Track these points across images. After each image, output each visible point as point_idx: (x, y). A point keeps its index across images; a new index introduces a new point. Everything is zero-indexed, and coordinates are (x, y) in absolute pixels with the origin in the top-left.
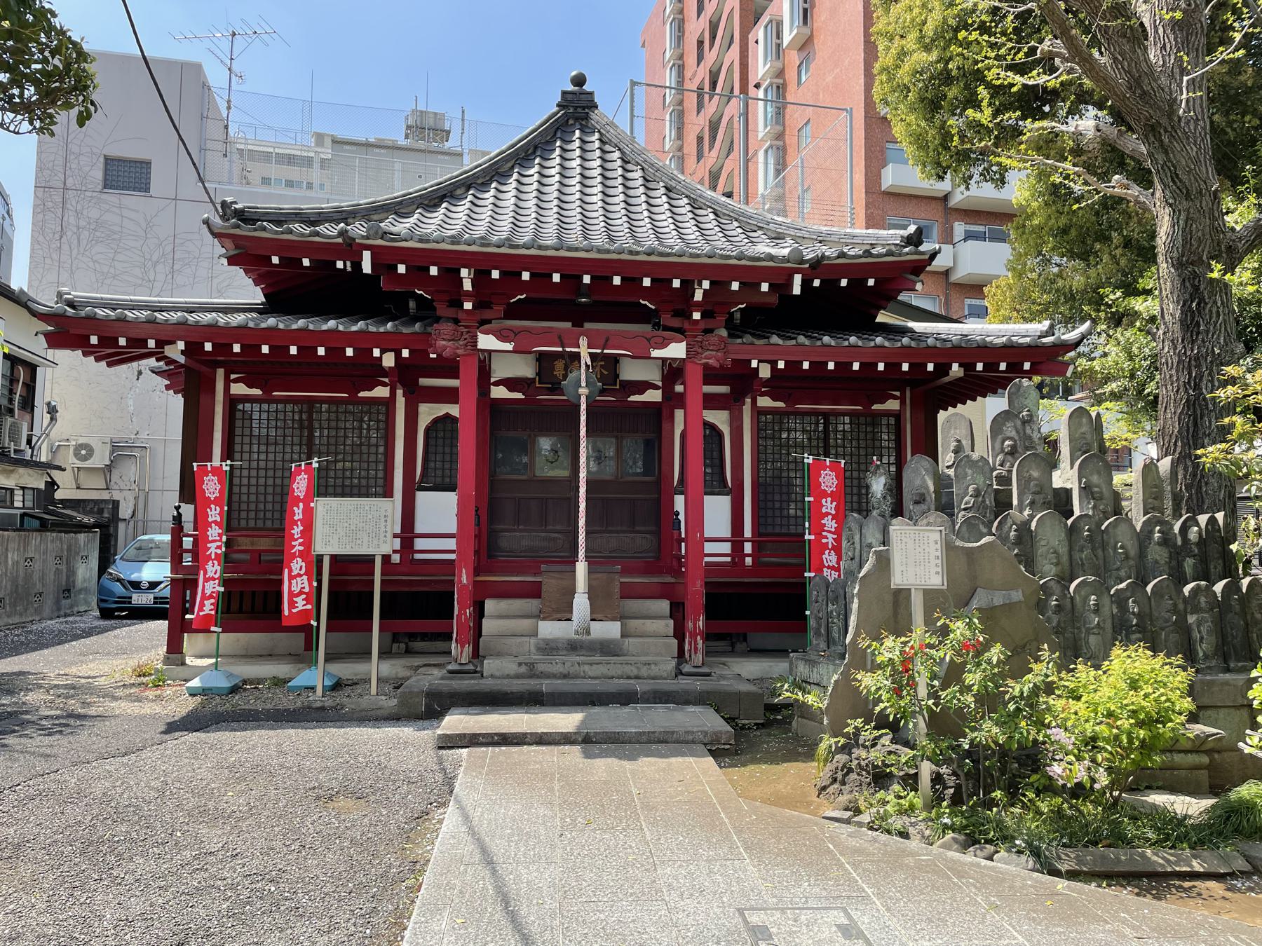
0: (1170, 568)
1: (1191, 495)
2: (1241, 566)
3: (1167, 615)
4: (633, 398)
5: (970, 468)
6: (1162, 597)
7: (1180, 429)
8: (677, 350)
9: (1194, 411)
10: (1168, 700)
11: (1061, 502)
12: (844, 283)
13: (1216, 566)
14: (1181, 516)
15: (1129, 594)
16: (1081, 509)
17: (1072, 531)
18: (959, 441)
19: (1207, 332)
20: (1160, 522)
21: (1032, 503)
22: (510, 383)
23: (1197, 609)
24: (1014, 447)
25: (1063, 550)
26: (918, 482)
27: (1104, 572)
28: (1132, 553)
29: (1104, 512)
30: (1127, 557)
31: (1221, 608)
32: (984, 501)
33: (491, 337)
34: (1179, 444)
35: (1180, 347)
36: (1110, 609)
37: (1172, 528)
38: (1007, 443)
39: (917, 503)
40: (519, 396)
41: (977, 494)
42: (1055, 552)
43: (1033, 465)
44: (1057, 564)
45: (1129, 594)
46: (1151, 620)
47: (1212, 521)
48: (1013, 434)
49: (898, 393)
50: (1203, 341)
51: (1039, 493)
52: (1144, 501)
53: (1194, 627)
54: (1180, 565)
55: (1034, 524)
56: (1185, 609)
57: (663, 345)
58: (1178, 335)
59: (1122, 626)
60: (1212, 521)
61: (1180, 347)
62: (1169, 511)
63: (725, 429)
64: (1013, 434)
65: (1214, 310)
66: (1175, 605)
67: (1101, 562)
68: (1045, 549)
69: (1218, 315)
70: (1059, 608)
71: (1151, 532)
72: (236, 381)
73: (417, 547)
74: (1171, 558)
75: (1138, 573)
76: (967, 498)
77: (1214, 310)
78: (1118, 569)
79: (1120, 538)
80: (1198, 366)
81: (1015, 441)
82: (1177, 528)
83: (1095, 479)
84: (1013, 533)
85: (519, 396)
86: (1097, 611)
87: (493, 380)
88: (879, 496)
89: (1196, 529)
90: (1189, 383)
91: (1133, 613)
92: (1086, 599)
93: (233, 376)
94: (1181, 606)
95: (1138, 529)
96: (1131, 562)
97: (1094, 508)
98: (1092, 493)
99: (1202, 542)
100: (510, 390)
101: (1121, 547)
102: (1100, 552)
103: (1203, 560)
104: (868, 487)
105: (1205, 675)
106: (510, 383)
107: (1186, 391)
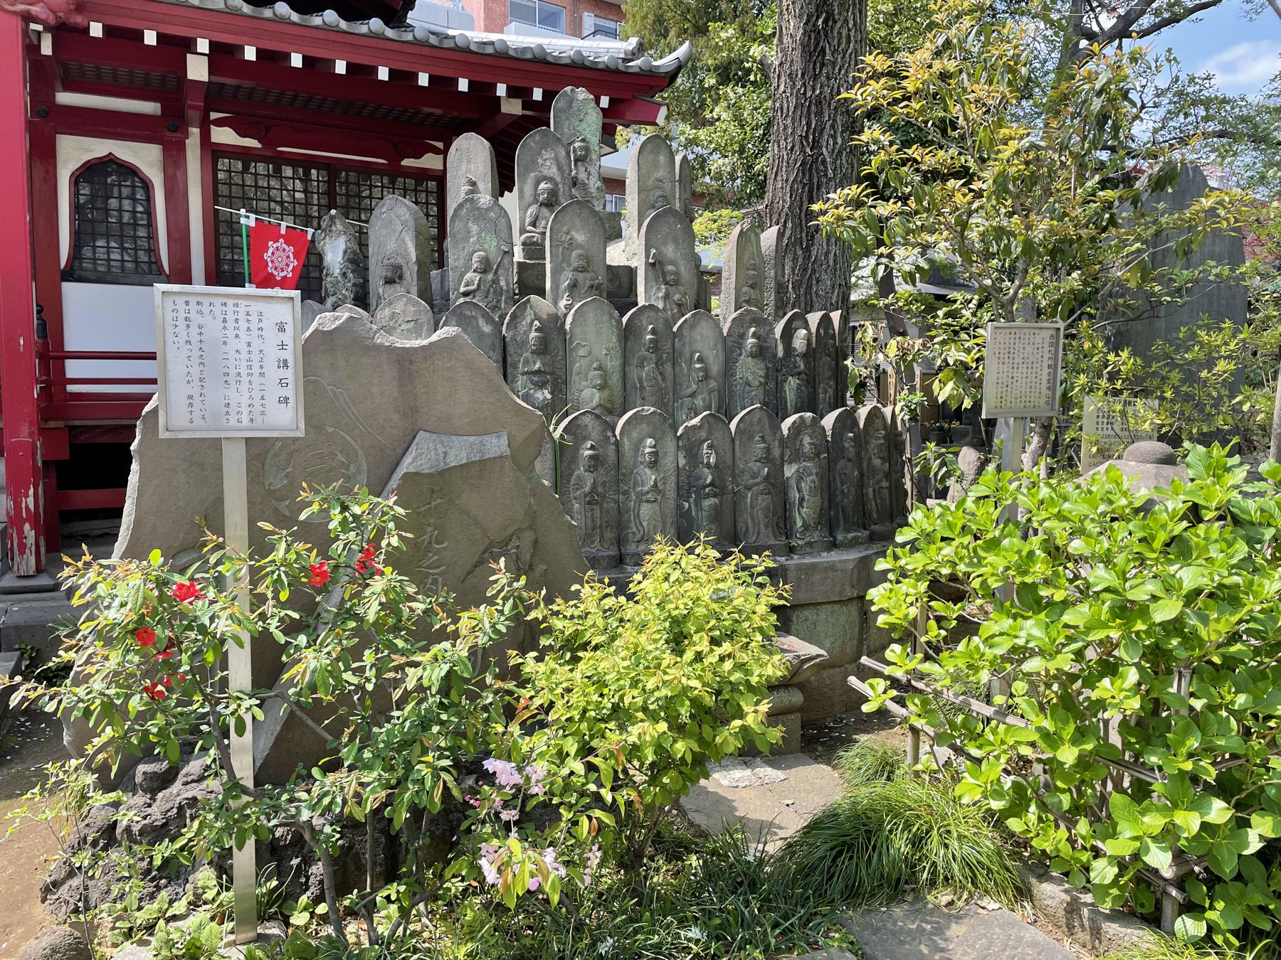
0: (766, 393)
1: (798, 296)
2: (852, 390)
3: (755, 466)
5: (476, 220)
6: (751, 437)
7: (792, 204)
9: (811, 179)
10: (740, 666)
11: (618, 289)
13: (825, 392)
14: (785, 314)
15: (703, 434)
16: (647, 298)
17: (628, 334)
18: (473, 184)
19: (834, 64)
20: (757, 321)
21: (573, 286)
23: (797, 456)
24: (553, 193)
25: (613, 364)
26: (391, 246)
27: (669, 404)
28: (715, 369)
29: (679, 305)
30: (707, 377)
31: (830, 451)
32: (495, 281)
34: (790, 225)
35: (799, 84)
36: (673, 458)
37: (772, 331)
38: (543, 186)
39: (389, 281)
41: (485, 267)
42: (600, 368)
43: (577, 222)
44: (601, 388)
45: (703, 434)
46: (733, 476)
47: (826, 321)
48: (553, 172)
49: (440, 145)
50: (828, 78)
51: (583, 270)
52: (738, 290)
53: (793, 483)
54: (779, 388)
55: (569, 319)
56: (782, 455)
58: (798, 66)
59: (690, 486)
60: (826, 321)
61: (799, 84)
62: (770, 309)
63: (98, 148)
64: (553, 172)
65: (844, 32)
66: (768, 450)
67: (669, 383)
68: (584, 362)
69: (849, 42)
70: (596, 462)
71: (743, 336)
73: (70, 374)
74: (767, 377)
75: (721, 400)
76: (469, 275)
77: (844, 32)
78: (693, 395)
79: (699, 345)
80: (819, 114)
81: (556, 184)
82: (779, 328)
83: (670, 251)
84: (533, 334)
86: (654, 464)
88: (337, 272)
89: (804, 332)
90: (806, 137)
91: (708, 465)
92: (638, 445)
94: (776, 452)
95: (725, 332)
96: (713, 384)
97: (667, 297)
98: (664, 274)
99: (810, 354)
101: (700, 360)
102: (668, 368)
103: (810, 381)
104: (320, 257)
105: (803, 555)
107: (803, 150)
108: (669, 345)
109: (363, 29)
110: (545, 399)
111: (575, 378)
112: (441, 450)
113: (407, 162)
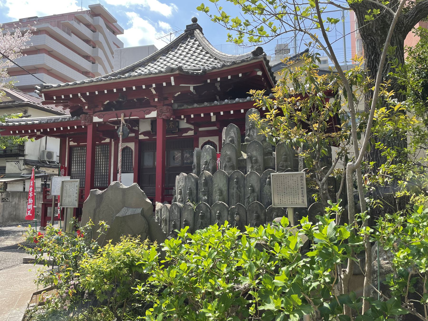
4: (184, 135)
6: (253, 212)
8: (154, 114)
12: (229, 77)
22: (145, 134)
25: (225, 189)
28: (257, 189)
33: (97, 117)
40: (147, 138)
51: (228, 162)
57: (149, 113)
72: (71, 141)
85: (147, 138)
87: (140, 133)
93: (70, 140)
96: (255, 194)
100: (145, 136)
106: (145, 134)
108: (243, 182)
109: (203, 105)
110: (205, 199)
111: (214, 193)
112: (126, 211)
113: (103, 142)
